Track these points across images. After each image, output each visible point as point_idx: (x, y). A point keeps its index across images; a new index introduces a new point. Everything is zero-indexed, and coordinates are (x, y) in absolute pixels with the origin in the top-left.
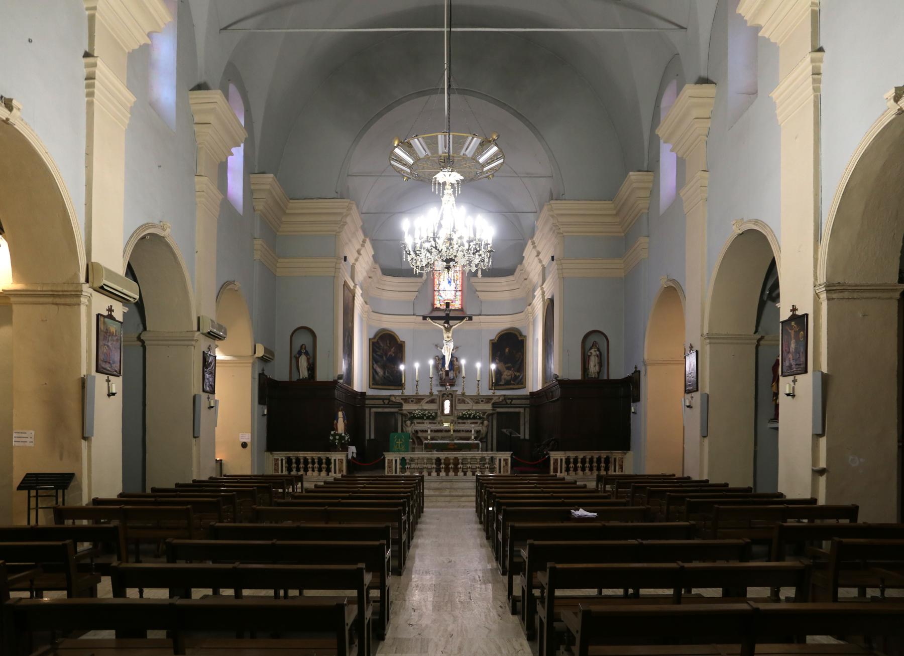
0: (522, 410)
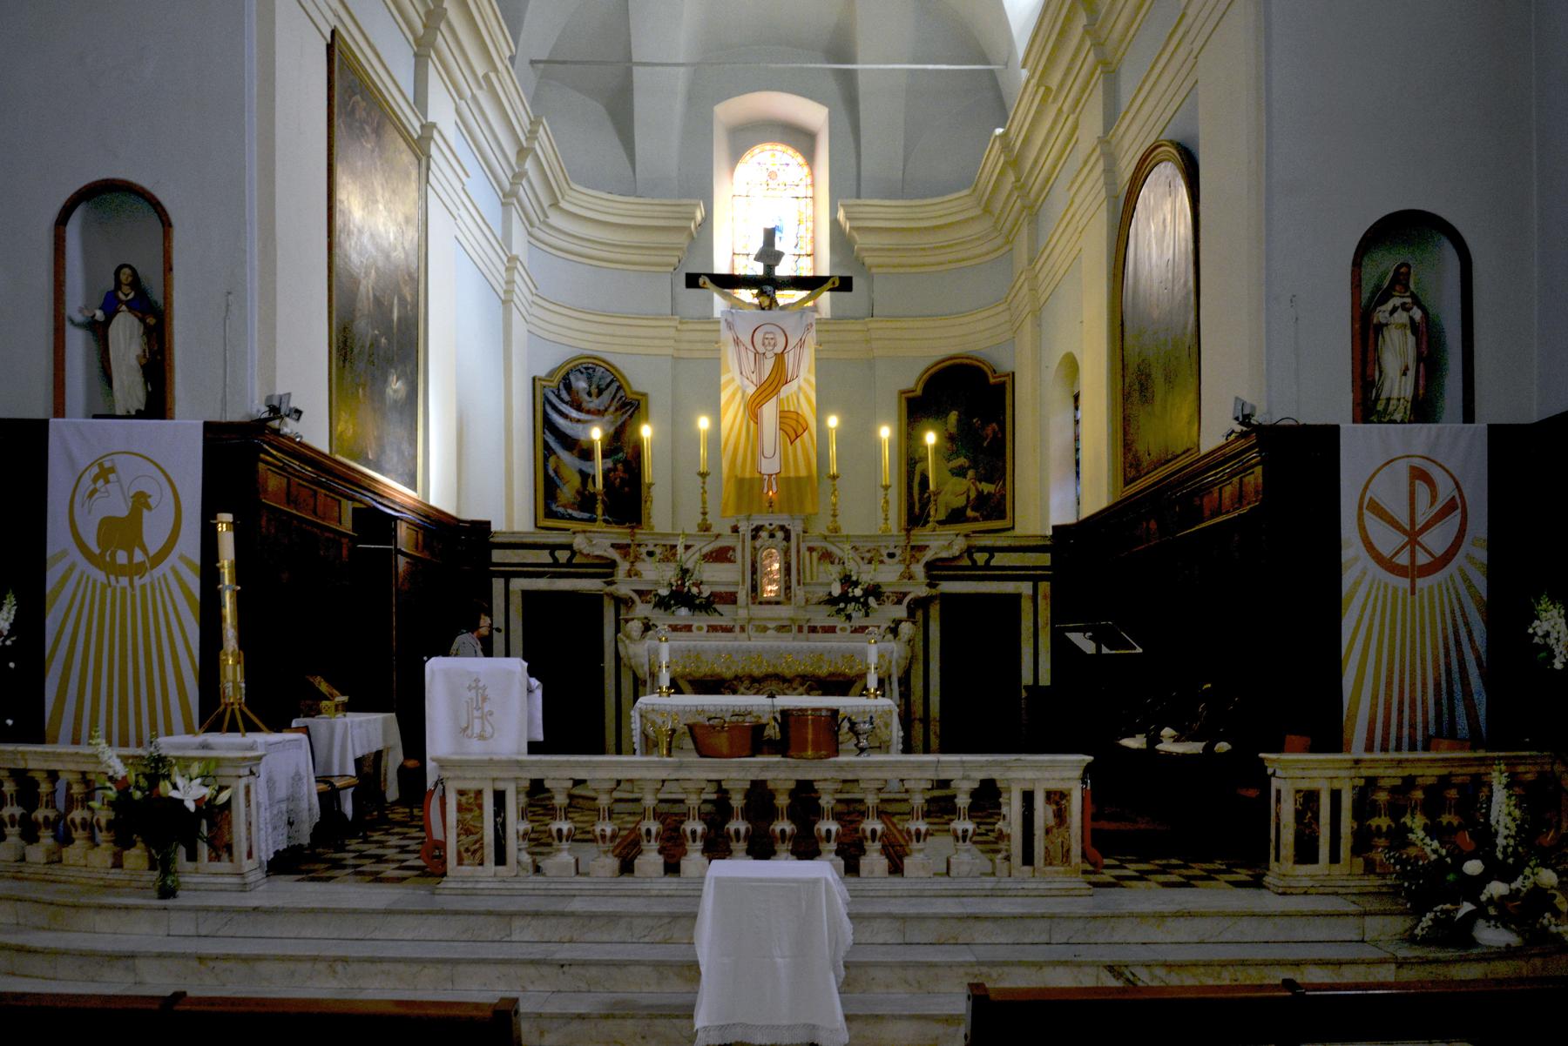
0: (1025, 588)
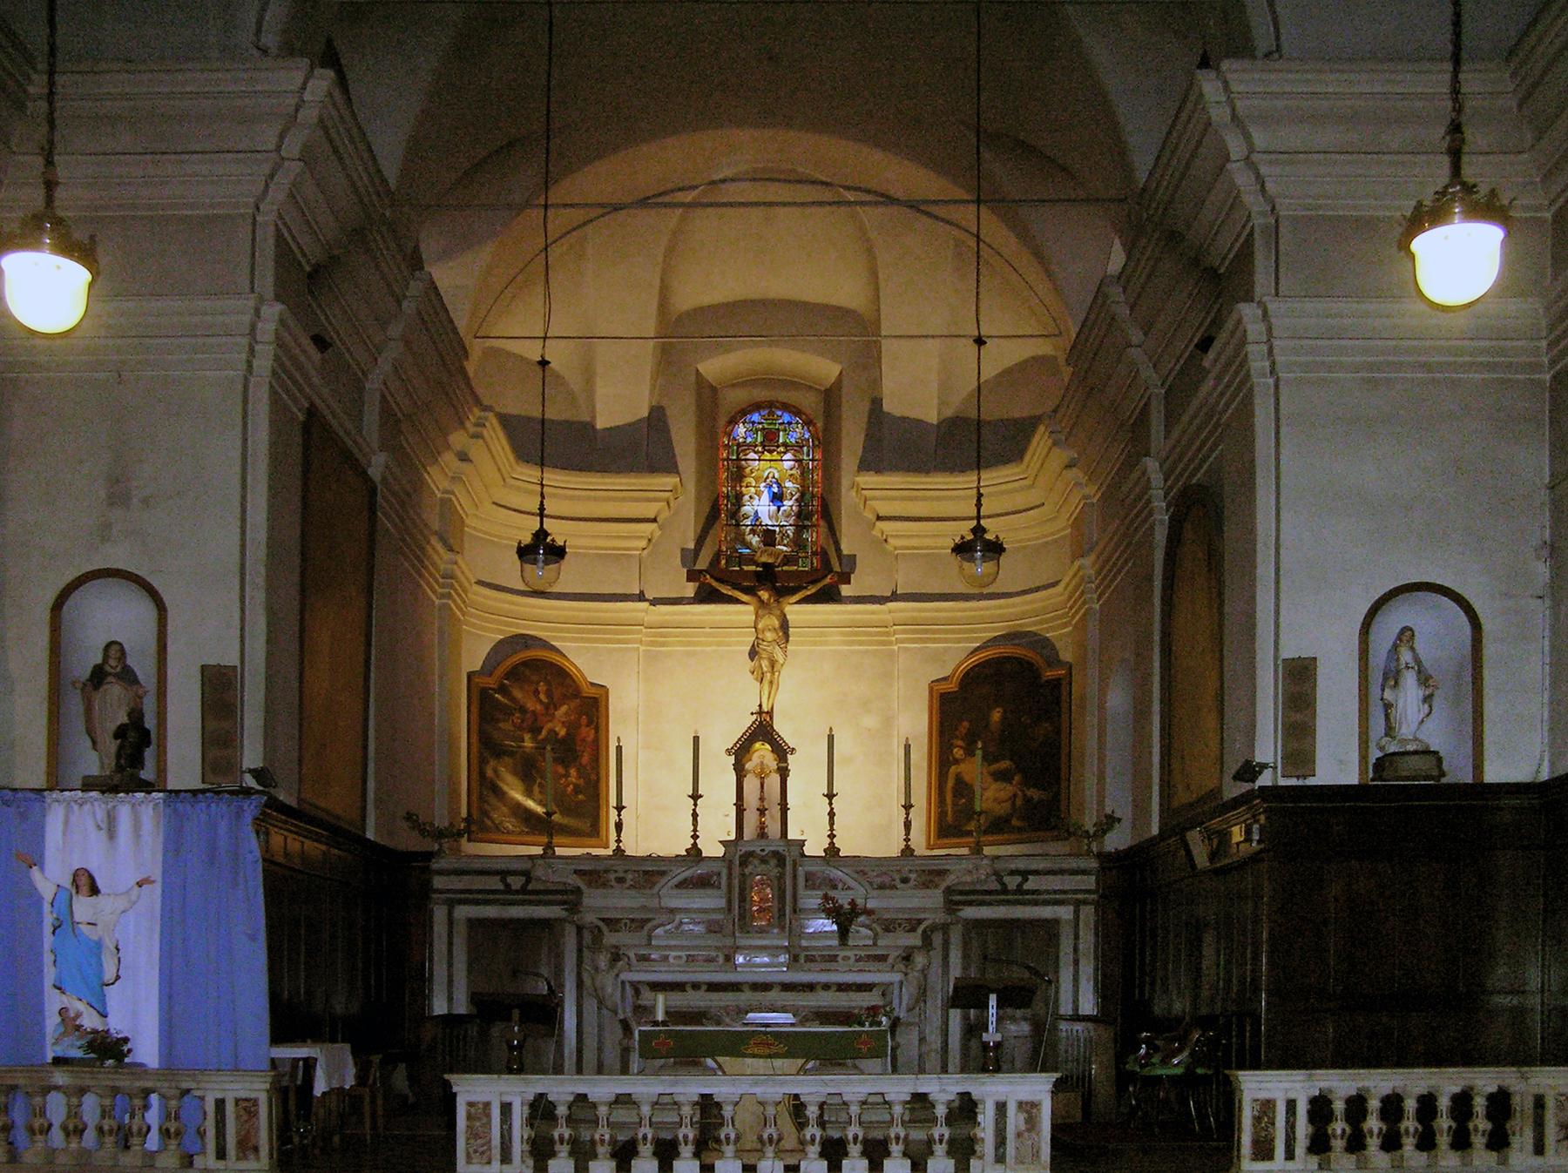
0: (1065, 913)
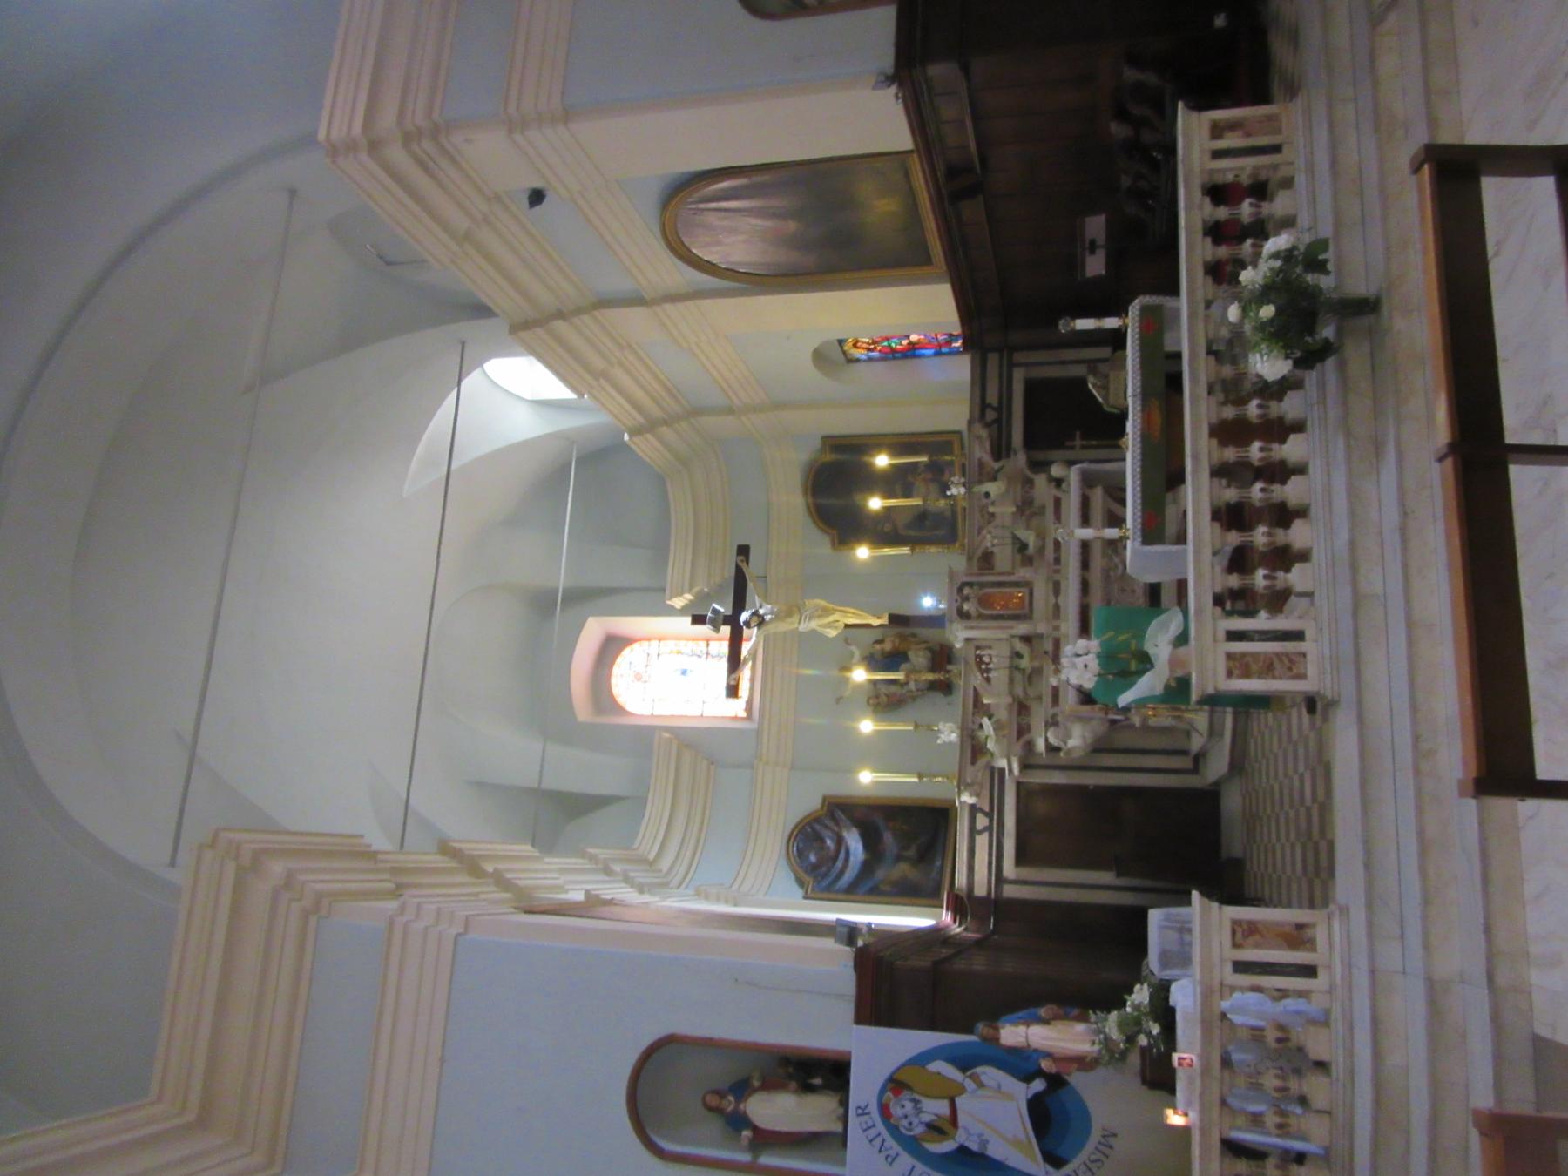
0: (1019, 376)
